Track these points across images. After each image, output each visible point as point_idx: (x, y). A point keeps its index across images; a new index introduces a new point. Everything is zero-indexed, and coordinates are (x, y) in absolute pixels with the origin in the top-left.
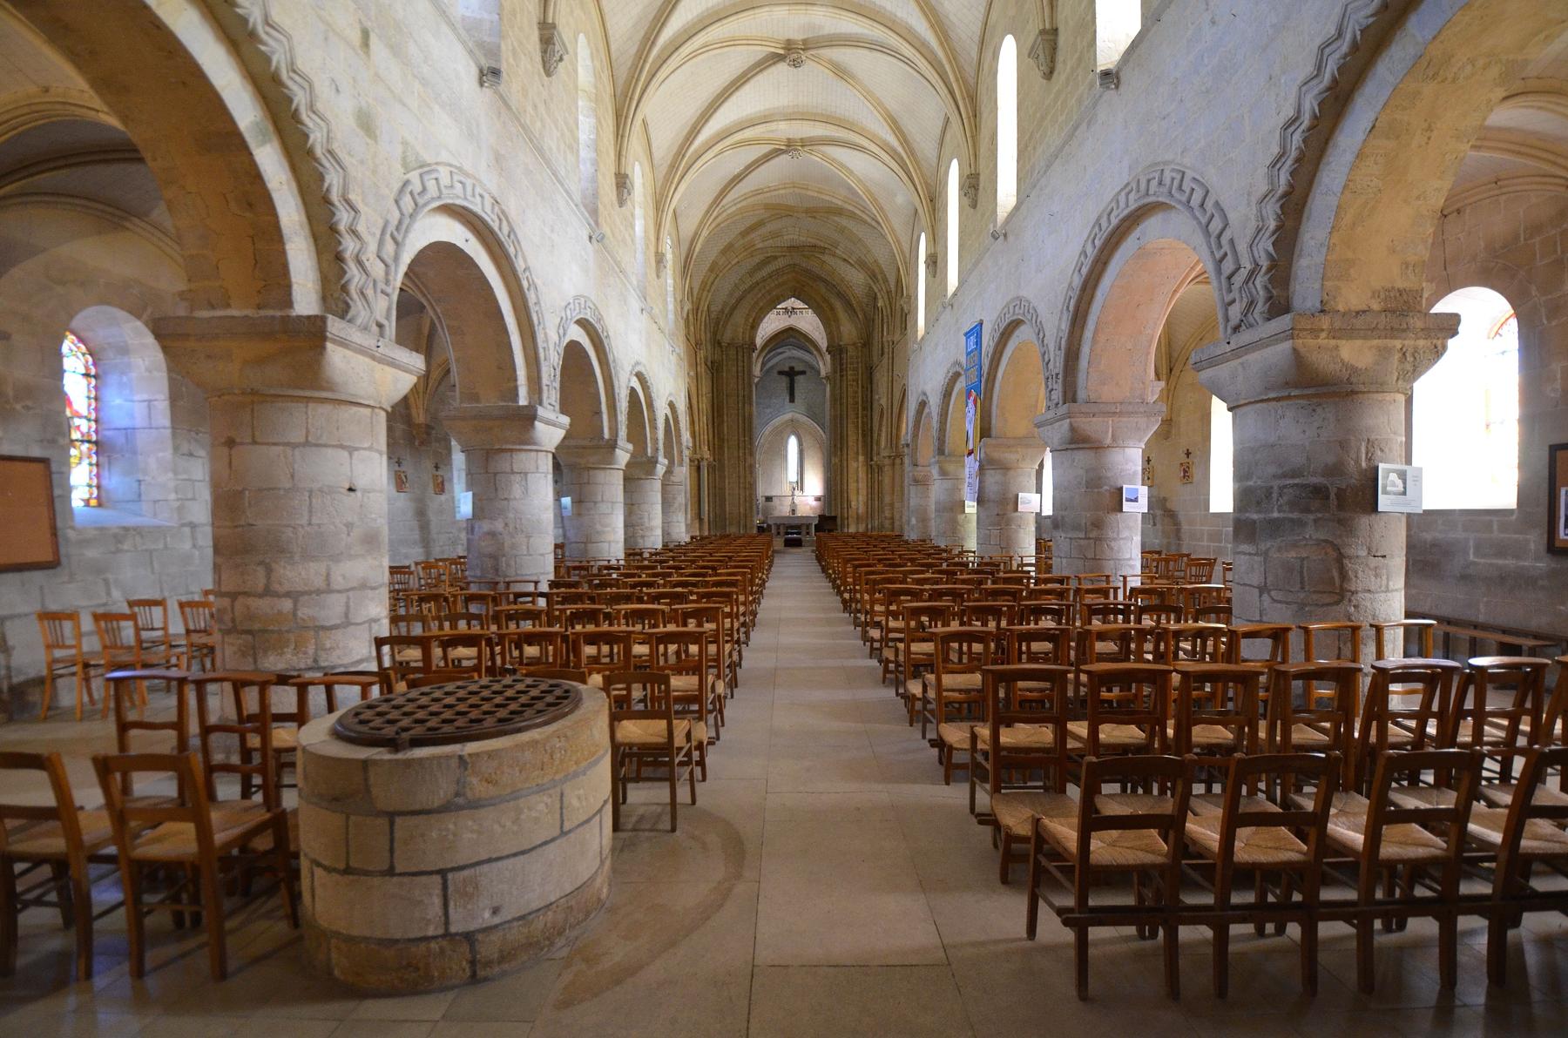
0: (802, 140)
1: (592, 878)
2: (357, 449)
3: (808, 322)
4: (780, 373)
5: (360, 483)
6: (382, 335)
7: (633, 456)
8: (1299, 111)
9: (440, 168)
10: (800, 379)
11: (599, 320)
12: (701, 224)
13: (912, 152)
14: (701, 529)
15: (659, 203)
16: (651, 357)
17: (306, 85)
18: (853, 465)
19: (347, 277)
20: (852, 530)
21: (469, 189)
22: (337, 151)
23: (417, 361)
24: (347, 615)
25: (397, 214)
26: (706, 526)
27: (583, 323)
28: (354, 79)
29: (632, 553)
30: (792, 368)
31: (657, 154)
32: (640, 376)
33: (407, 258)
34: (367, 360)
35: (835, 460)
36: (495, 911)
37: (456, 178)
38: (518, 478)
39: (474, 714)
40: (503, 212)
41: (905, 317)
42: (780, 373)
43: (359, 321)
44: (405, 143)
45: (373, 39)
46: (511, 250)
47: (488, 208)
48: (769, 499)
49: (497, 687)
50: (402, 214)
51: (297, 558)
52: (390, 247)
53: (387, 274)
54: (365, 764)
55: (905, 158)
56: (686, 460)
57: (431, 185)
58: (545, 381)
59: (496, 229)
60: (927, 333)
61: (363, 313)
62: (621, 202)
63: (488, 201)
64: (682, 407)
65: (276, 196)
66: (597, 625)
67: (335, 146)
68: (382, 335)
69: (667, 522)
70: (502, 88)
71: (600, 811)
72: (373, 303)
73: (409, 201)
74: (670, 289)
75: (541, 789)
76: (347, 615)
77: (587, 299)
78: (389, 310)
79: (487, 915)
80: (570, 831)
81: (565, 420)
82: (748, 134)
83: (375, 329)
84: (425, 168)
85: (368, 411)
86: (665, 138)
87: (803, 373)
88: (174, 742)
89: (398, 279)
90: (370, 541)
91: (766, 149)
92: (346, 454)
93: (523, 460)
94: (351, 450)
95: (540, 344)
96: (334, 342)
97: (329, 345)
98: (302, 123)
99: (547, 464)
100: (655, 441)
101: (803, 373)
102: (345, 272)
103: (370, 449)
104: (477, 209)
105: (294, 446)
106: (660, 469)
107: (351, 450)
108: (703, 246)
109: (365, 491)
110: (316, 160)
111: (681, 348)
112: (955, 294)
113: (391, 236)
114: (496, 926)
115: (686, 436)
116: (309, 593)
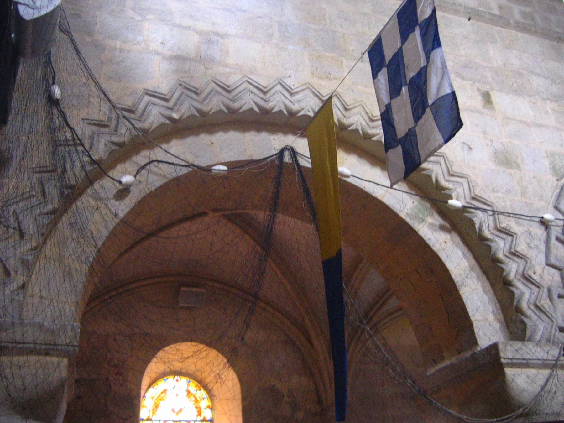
28: (484, 133)
45: (495, 96)
61: (541, 327)
65: (442, 256)
66: (436, 404)
91: (530, 285)
96: (513, 365)
97: (508, 371)
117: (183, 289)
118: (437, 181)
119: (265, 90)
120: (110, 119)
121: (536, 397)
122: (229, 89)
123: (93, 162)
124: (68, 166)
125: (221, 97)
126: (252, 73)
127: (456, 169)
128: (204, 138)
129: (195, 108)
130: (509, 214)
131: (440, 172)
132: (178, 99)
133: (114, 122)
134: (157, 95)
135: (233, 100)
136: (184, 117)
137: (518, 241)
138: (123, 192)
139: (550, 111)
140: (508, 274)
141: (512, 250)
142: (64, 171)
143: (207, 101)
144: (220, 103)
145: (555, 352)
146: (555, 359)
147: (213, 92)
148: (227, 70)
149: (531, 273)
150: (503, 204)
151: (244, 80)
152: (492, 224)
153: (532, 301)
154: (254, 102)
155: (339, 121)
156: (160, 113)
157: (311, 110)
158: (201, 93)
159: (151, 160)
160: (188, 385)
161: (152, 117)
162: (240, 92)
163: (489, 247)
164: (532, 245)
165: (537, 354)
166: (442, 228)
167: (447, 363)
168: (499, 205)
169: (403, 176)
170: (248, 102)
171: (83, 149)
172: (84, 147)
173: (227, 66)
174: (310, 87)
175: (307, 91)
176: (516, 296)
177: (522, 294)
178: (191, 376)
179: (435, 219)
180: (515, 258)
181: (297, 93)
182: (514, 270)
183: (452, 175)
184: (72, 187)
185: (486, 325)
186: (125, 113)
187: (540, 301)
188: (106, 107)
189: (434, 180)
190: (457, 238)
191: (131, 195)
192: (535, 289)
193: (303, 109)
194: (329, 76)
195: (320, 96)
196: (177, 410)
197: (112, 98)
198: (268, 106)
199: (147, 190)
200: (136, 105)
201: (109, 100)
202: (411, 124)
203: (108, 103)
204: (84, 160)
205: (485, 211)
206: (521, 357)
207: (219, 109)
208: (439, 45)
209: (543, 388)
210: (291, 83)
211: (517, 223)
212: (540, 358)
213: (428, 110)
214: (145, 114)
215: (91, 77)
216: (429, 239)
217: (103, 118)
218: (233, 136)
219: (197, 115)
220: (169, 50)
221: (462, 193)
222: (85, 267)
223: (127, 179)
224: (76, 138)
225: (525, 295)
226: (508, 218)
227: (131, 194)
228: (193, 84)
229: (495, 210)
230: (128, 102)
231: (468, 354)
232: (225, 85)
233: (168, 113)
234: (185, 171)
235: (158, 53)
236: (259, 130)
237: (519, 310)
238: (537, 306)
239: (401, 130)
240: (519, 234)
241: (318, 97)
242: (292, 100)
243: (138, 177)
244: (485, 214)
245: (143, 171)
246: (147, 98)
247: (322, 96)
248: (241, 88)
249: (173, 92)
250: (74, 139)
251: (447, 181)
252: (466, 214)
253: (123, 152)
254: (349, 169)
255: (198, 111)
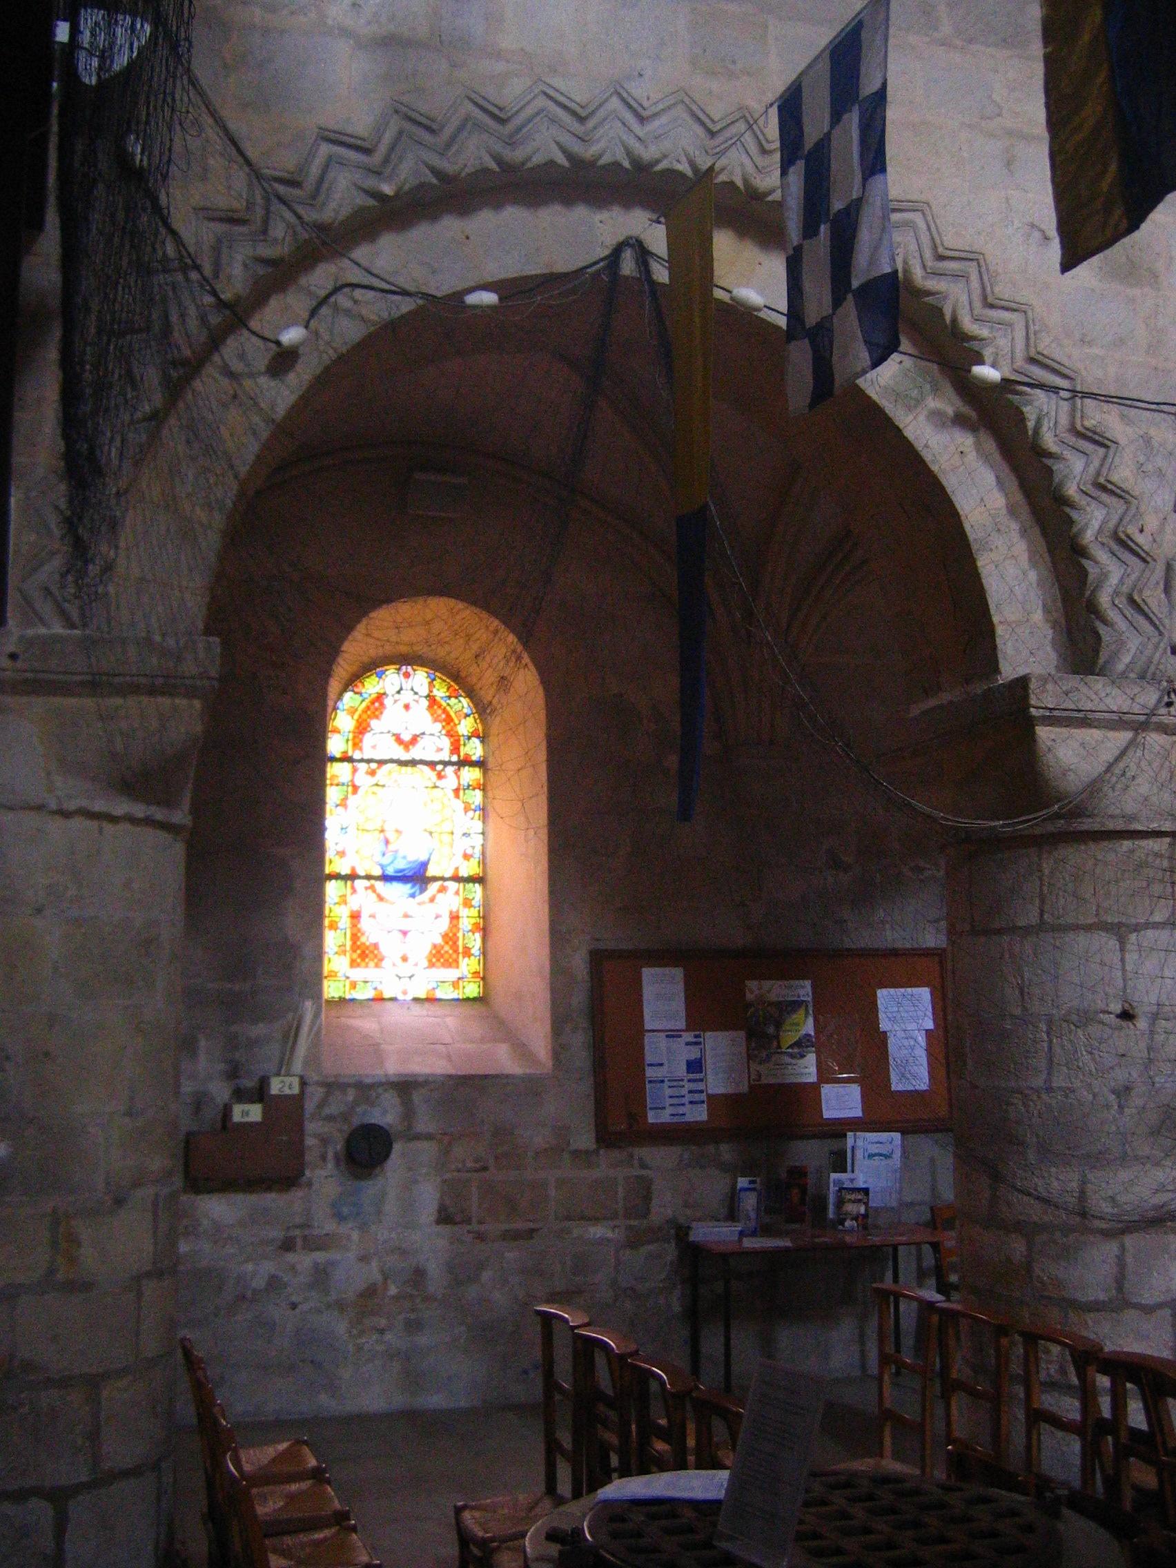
5: (1146, 997)
8: (864, 186)
22: (1057, 354)
24: (1120, 1281)
51: (1032, 1157)
65: (950, 482)
76: (1120, 1281)
88: (44, 1504)
91: (1127, 556)
94: (1120, 931)
96: (1052, 721)
97: (1043, 732)
105: (1027, 931)
107: (1120, 931)
117: (418, 476)
118: (954, 320)
119: (583, 113)
120: (250, 206)
121: (1094, 781)
122: (502, 115)
123: (221, 304)
124: (174, 318)
125: (485, 136)
126: (553, 70)
127: (1002, 290)
128: (450, 226)
129: (428, 166)
130: (1108, 399)
131: (964, 298)
132: (392, 148)
133: (259, 212)
134: (345, 139)
135: (511, 142)
136: (406, 187)
137: (1117, 460)
138: (284, 359)
140: (1082, 531)
141: (1102, 480)
142: (167, 330)
143: (454, 149)
144: (484, 153)
145: (1150, 697)
146: (1148, 711)
147: (469, 126)
148: (500, 67)
149: (1132, 530)
150: (1100, 373)
151: (536, 91)
152: (1064, 421)
153: (1125, 589)
154: (558, 143)
155: (745, 181)
156: (355, 185)
157: (684, 159)
158: (442, 127)
159: (340, 283)
160: (431, 684)
161: (337, 196)
162: (524, 126)
163: (1050, 471)
164: (1149, 467)
165: (1108, 700)
166: (960, 421)
167: (945, 697)
168: (1091, 376)
169: (808, 401)
170: (544, 145)
171: (199, 276)
172: (202, 274)
173: (498, 55)
174: (687, 100)
175: (680, 107)
176: (1090, 578)
177: (1105, 576)
178: (437, 666)
179: (947, 403)
180: (1104, 497)
181: (656, 115)
182: (1095, 524)
183: (992, 306)
184: (185, 363)
185: (1023, 635)
186: (281, 189)
187: (1141, 591)
188: (240, 178)
189: (948, 318)
190: (990, 445)
191: (299, 367)
193: (665, 156)
194: (731, 67)
195: (707, 121)
196: (406, 737)
197: (252, 153)
198: (589, 152)
199: (331, 352)
200: (302, 168)
201: (248, 162)
202: (827, 310)
203: (247, 169)
204: (205, 302)
205: (1055, 390)
206: (1072, 706)
207: (479, 167)
208: (883, 170)
209: (1110, 767)
210: (639, 91)
211: (1122, 416)
212: (1115, 709)
213: (850, 297)
214: (326, 185)
215: (207, 107)
216: (926, 446)
217: (236, 205)
218: (513, 215)
219: (434, 181)
220: (369, 23)
221: (1007, 349)
222: (219, 520)
223: (292, 336)
224: (185, 254)
225: (1110, 574)
226: (1106, 407)
227: (300, 361)
228: (423, 107)
229: (1079, 389)
230: (287, 161)
231: (979, 688)
232: (496, 106)
233: (371, 182)
234: (406, 306)
235: (344, 32)
236: (568, 202)
237: (1092, 608)
238: (1132, 601)
239: (812, 316)
240: (1123, 441)
241: (703, 124)
242: (641, 134)
243: (313, 324)
244: (1054, 396)
245: (324, 311)
246: (325, 149)
247: (712, 121)
248: (529, 111)
249: (379, 131)
250: (181, 258)
251: (976, 320)
252: (1010, 396)
253: (279, 275)
254: (761, 292)
255: (435, 172)
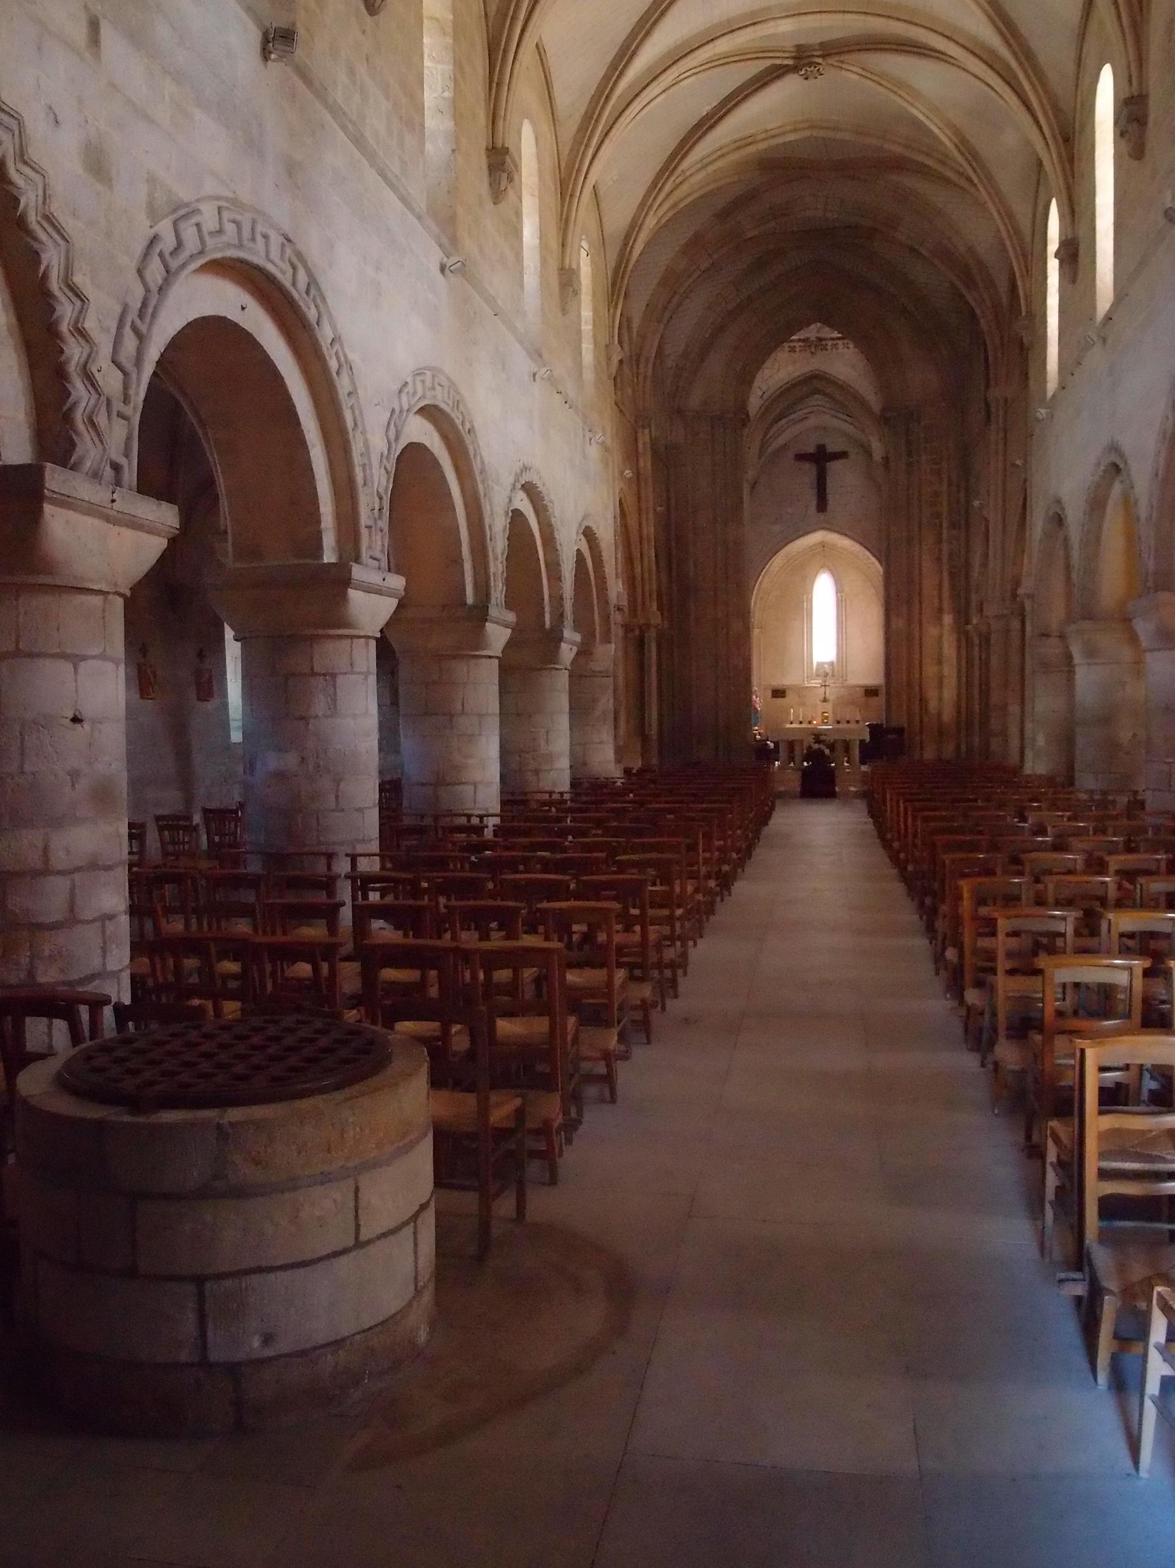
0: (822, 45)
1: (403, 1313)
2: (84, 658)
3: (845, 363)
4: (801, 457)
5: (87, 711)
6: (118, 482)
7: (516, 629)
9: (203, 207)
10: (835, 468)
11: (457, 404)
12: (644, 207)
13: (1026, 55)
14: (644, 753)
15: (566, 181)
16: (547, 450)
17: (14, 125)
18: (932, 631)
19: (71, 400)
20: (929, 754)
21: (246, 232)
23: (166, 516)
24: (72, 908)
25: (139, 292)
26: (654, 751)
27: (430, 412)
28: (80, 101)
29: (514, 798)
30: (821, 448)
31: (563, 99)
32: (530, 490)
33: (154, 353)
34: (97, 522)
35: (899, 623)
36: (268, 1339)
37: (226, 215)
38: (320, 683)
39: (239, 1068)
40: (299, 255)
41: (1027, 349)
42: (801, 457)
43: (88, 464)
44: (152, 180)
45: (107, 32)
46: (312, 314)
47: (275, 254)
48: (779, 693)
49: (272, 1031)
50: (148, 290)
52: (130, 343)
53: (126, 386)
54: (100, 1124)
55: (1015, 59)
56: (617, 632)
57: (189, 233)
58: (364, 519)
59: (287, 284)
60: (1062, 387)
61: (92, 453)
62: (497, 195)
63: (276, 240)
64: (607, 533)
67: (55, 208)
68: (118, 482)
69: (577, 745)
70: (299, 52)
71: (415, 1217)
72: (106, 438)
73: (161, 263)
74: (587, 327)
75: (326, 1179)
76: (72, 908)
77: (436, 371)
78: (129, 439)
79: (256, 1342)
80: (369, 1242)
81: (397, 582)
82: (723, 46)
83: (108, 472)
84: (183, 213)
85: (97, 600)
86: (575, 77)
87: (843, 455)
89: (139, 393)
90: (102, 795)
91: (755, 68)
92: (69, 667)
93: (331, 653)
95: (357, 459)
97: (48, 508)
98: (10, 183)
99: (366, 657)
100: (558, 600)
101: (843, 455)
102: (69, 394)
103: (103, 657)
104: (258, 260)
106: (567, 652)
107: (76, 660)
108: (648, 244)
109: (94, 722)
110: (29, 233)
111: (606, 429)
112: (1108, 318)
113: (127, 308)
114: (270, 1360)
115: (616, 589)
116: (19, 874)
139: (167, 97)
140: (67, 361)
149: (94, 370)
183: (25, 163)
192: (95, 396)
